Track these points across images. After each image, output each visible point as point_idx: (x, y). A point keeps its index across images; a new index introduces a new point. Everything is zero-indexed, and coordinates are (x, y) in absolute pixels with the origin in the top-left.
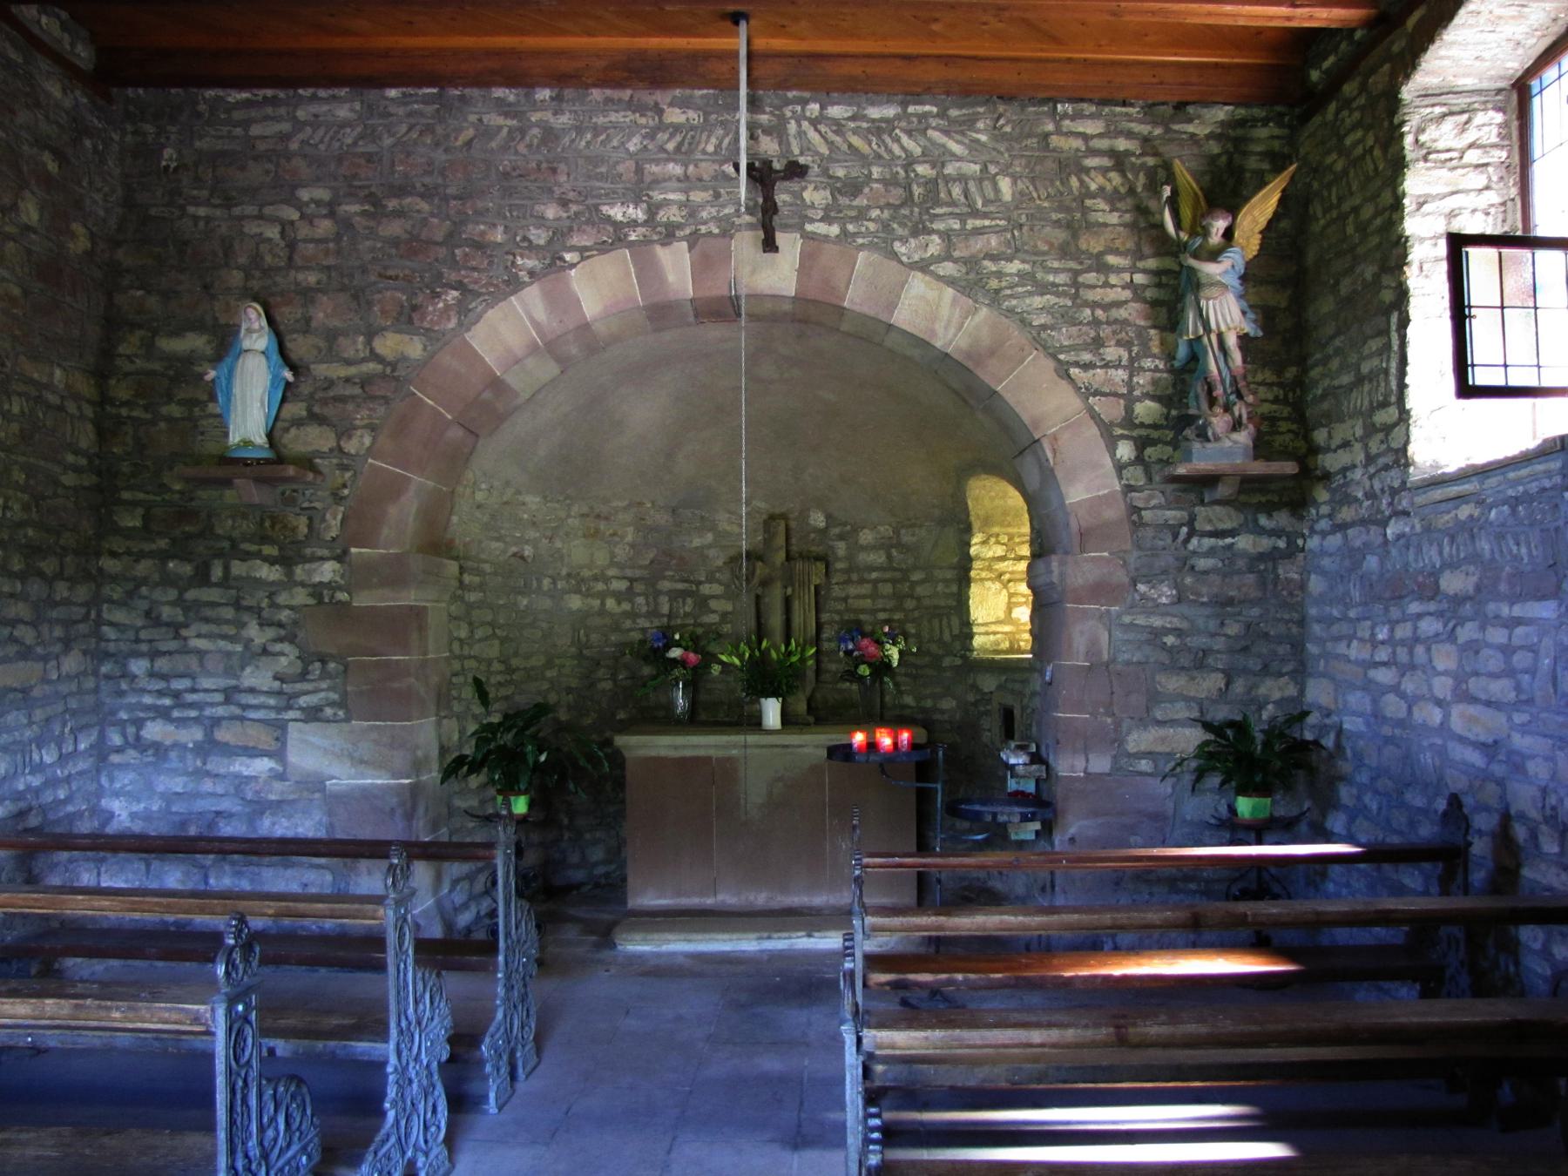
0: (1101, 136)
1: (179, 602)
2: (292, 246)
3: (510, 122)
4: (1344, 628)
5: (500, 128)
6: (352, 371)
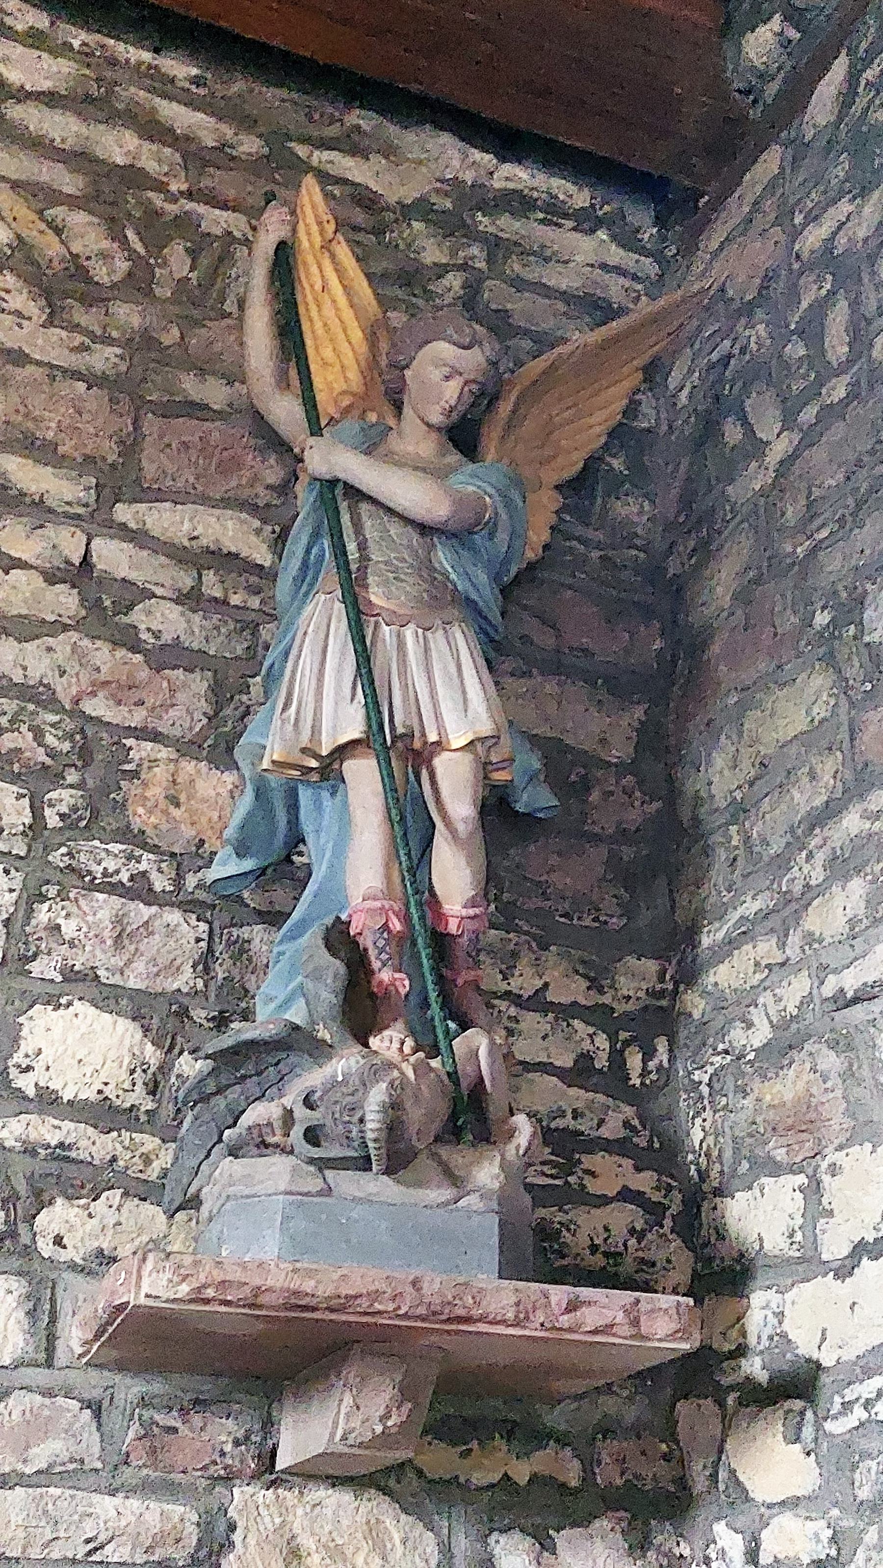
0: (50, 99)
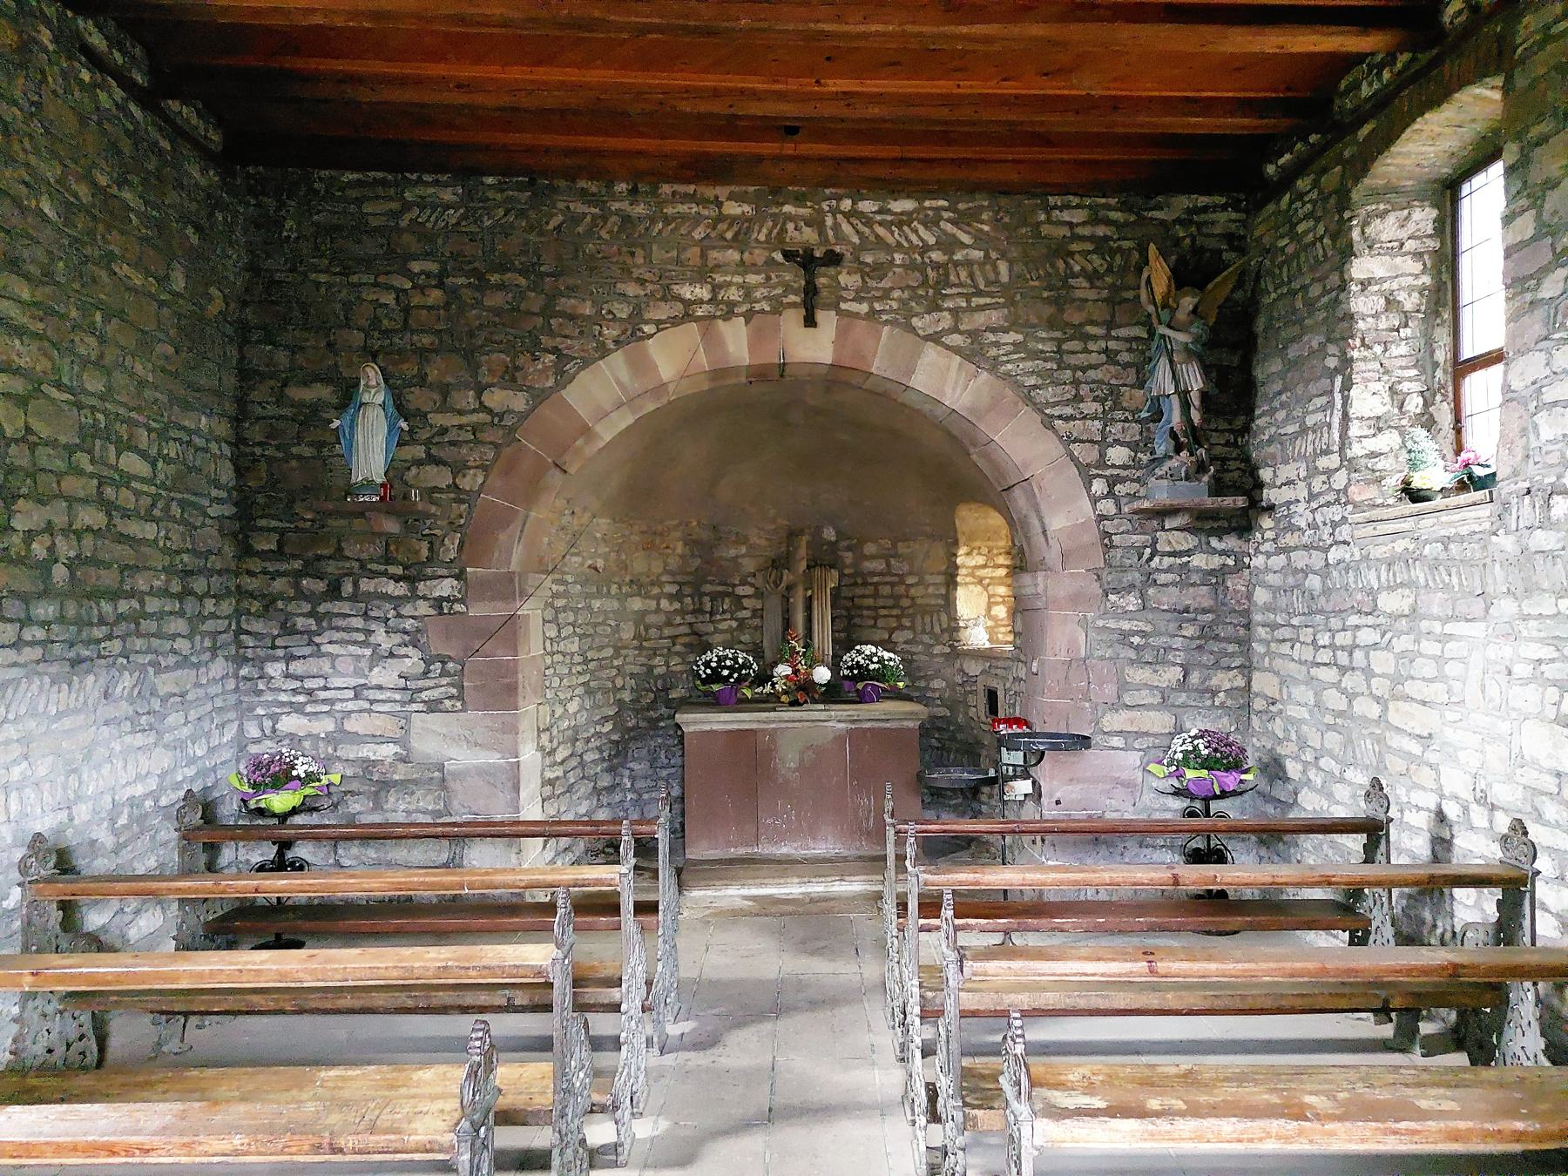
0: (1084, 224)
1: (312, 614)
2: (407, 310)
3: (593, 210)
4: (1286, 633)
5: (585, 215)
6: (464, 420)
